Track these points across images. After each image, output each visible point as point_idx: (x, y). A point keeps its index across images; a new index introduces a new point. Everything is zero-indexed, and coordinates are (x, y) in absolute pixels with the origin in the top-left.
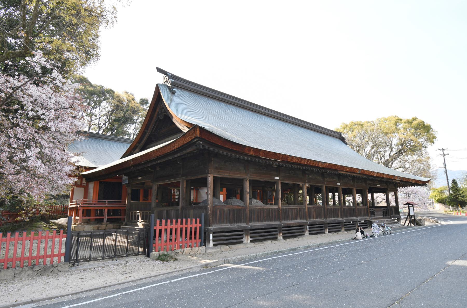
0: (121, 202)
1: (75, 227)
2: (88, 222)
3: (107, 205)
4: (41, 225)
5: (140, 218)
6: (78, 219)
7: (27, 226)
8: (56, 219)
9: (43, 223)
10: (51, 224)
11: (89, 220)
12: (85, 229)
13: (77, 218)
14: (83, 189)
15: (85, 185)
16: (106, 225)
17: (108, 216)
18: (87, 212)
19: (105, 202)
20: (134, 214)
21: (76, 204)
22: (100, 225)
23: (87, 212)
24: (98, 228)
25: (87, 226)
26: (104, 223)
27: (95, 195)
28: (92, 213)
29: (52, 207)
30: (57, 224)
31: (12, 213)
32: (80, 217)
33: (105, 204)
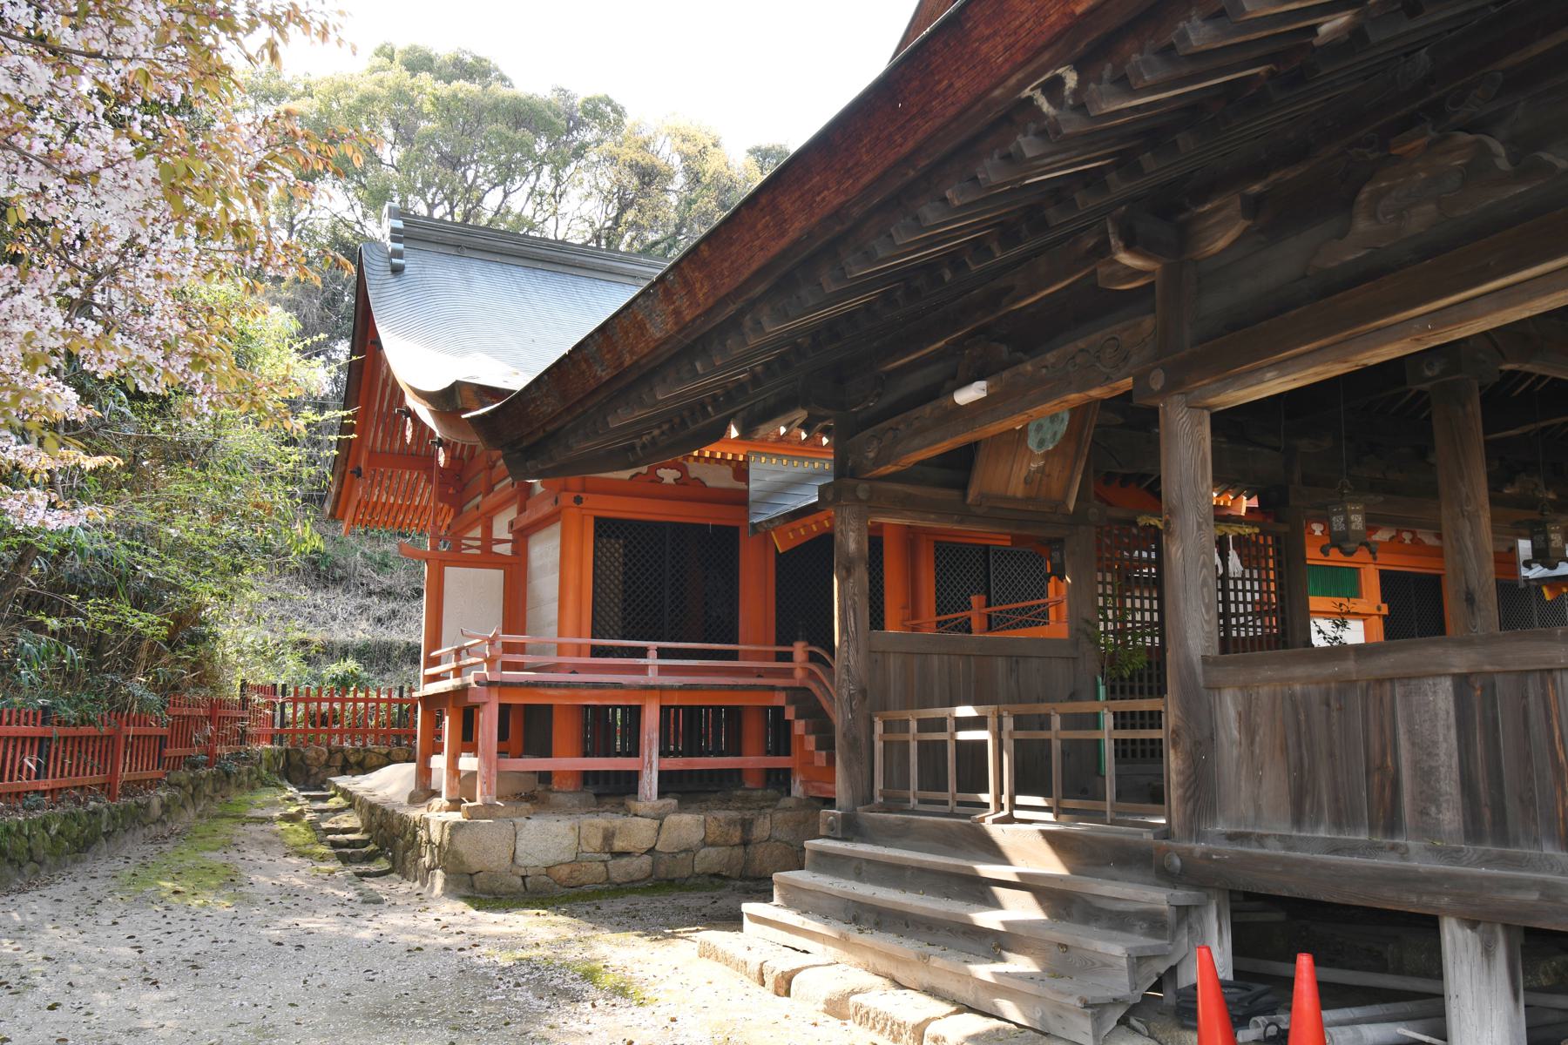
0: (733, 655)
1: (456, 827)
2: (536, 794)
3: (652, 677)
4: (274, 804)
5: (1000, 767)
6: (472, 775)
7: (190, 814)
8: (364, 768)
9: (292, 791)
10: (332, 803)
11: (545, 777)
12: (520, 847)
13: (468, 763)
14: (497, 576)
15: (505, 549)
16: (660, 818)
17: (663, 753)
18: (527, 727)
19: (642, 653)
20: (913, 736)
21: (458, 672)
22: (617, 821)
23: (527, 727)
24: (608, 836)
25: (534, 823)
26: (640, 806)
27: (572, 572)
28: (564, 731)
29: (343, 701)
30: (362, 801)
31: (56, 731)
32: (486, 760)
33: (643, 670)
